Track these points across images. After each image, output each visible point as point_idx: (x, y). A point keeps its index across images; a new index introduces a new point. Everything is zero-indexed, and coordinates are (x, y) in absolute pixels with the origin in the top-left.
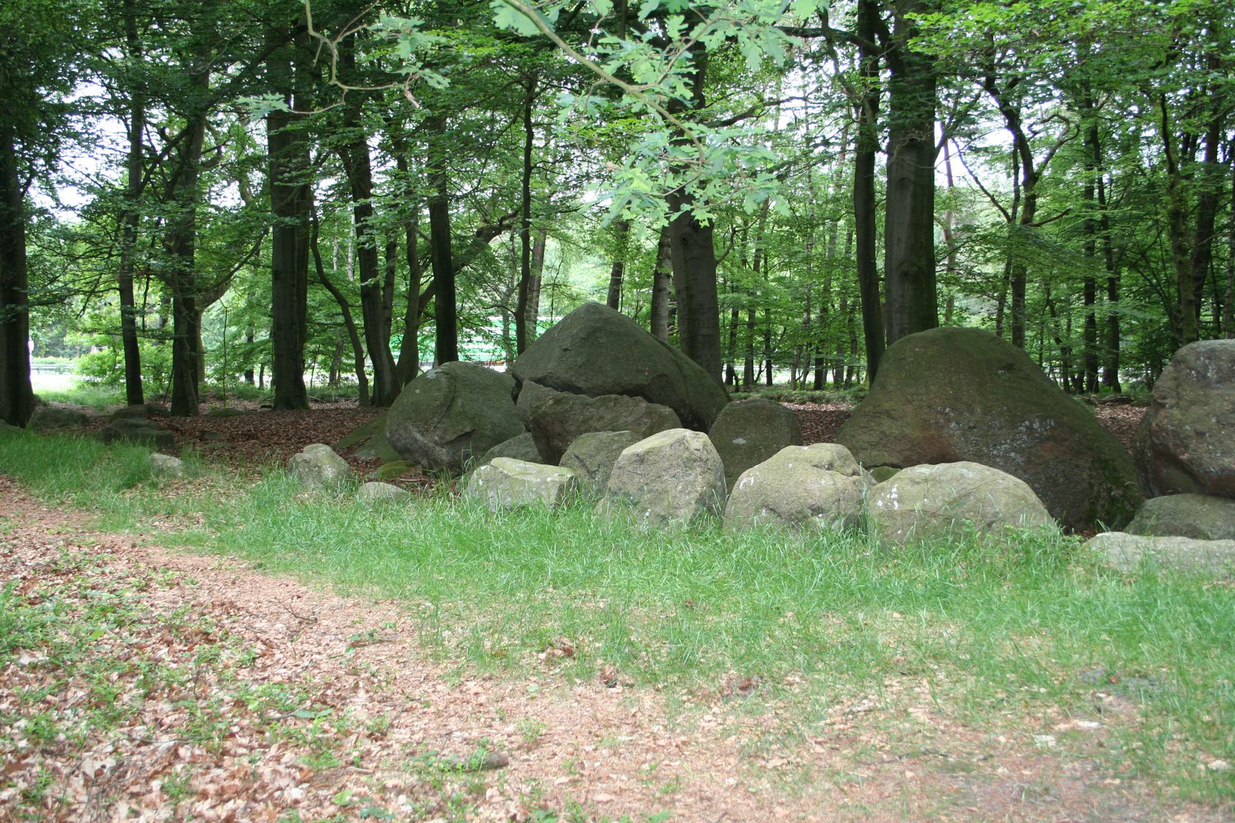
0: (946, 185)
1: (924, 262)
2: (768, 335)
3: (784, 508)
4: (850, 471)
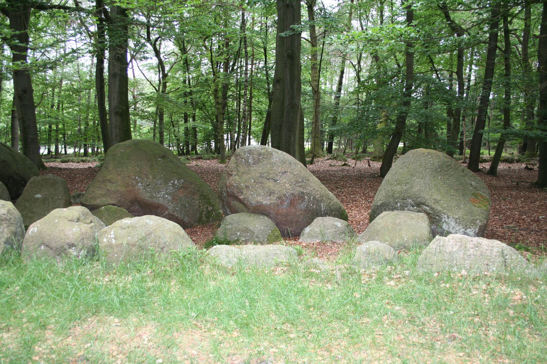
0: (132, 77)
1: (124, 108)
2: (64, 135)
3: (53, 245)
4: (89, 221)
